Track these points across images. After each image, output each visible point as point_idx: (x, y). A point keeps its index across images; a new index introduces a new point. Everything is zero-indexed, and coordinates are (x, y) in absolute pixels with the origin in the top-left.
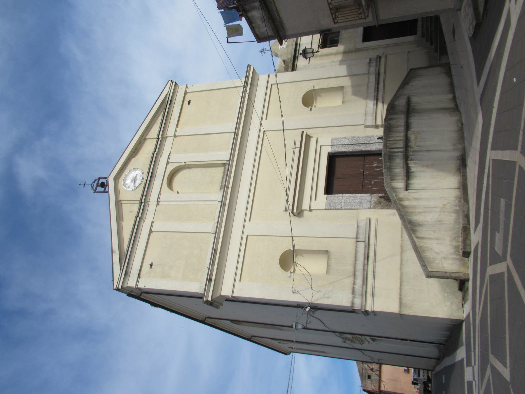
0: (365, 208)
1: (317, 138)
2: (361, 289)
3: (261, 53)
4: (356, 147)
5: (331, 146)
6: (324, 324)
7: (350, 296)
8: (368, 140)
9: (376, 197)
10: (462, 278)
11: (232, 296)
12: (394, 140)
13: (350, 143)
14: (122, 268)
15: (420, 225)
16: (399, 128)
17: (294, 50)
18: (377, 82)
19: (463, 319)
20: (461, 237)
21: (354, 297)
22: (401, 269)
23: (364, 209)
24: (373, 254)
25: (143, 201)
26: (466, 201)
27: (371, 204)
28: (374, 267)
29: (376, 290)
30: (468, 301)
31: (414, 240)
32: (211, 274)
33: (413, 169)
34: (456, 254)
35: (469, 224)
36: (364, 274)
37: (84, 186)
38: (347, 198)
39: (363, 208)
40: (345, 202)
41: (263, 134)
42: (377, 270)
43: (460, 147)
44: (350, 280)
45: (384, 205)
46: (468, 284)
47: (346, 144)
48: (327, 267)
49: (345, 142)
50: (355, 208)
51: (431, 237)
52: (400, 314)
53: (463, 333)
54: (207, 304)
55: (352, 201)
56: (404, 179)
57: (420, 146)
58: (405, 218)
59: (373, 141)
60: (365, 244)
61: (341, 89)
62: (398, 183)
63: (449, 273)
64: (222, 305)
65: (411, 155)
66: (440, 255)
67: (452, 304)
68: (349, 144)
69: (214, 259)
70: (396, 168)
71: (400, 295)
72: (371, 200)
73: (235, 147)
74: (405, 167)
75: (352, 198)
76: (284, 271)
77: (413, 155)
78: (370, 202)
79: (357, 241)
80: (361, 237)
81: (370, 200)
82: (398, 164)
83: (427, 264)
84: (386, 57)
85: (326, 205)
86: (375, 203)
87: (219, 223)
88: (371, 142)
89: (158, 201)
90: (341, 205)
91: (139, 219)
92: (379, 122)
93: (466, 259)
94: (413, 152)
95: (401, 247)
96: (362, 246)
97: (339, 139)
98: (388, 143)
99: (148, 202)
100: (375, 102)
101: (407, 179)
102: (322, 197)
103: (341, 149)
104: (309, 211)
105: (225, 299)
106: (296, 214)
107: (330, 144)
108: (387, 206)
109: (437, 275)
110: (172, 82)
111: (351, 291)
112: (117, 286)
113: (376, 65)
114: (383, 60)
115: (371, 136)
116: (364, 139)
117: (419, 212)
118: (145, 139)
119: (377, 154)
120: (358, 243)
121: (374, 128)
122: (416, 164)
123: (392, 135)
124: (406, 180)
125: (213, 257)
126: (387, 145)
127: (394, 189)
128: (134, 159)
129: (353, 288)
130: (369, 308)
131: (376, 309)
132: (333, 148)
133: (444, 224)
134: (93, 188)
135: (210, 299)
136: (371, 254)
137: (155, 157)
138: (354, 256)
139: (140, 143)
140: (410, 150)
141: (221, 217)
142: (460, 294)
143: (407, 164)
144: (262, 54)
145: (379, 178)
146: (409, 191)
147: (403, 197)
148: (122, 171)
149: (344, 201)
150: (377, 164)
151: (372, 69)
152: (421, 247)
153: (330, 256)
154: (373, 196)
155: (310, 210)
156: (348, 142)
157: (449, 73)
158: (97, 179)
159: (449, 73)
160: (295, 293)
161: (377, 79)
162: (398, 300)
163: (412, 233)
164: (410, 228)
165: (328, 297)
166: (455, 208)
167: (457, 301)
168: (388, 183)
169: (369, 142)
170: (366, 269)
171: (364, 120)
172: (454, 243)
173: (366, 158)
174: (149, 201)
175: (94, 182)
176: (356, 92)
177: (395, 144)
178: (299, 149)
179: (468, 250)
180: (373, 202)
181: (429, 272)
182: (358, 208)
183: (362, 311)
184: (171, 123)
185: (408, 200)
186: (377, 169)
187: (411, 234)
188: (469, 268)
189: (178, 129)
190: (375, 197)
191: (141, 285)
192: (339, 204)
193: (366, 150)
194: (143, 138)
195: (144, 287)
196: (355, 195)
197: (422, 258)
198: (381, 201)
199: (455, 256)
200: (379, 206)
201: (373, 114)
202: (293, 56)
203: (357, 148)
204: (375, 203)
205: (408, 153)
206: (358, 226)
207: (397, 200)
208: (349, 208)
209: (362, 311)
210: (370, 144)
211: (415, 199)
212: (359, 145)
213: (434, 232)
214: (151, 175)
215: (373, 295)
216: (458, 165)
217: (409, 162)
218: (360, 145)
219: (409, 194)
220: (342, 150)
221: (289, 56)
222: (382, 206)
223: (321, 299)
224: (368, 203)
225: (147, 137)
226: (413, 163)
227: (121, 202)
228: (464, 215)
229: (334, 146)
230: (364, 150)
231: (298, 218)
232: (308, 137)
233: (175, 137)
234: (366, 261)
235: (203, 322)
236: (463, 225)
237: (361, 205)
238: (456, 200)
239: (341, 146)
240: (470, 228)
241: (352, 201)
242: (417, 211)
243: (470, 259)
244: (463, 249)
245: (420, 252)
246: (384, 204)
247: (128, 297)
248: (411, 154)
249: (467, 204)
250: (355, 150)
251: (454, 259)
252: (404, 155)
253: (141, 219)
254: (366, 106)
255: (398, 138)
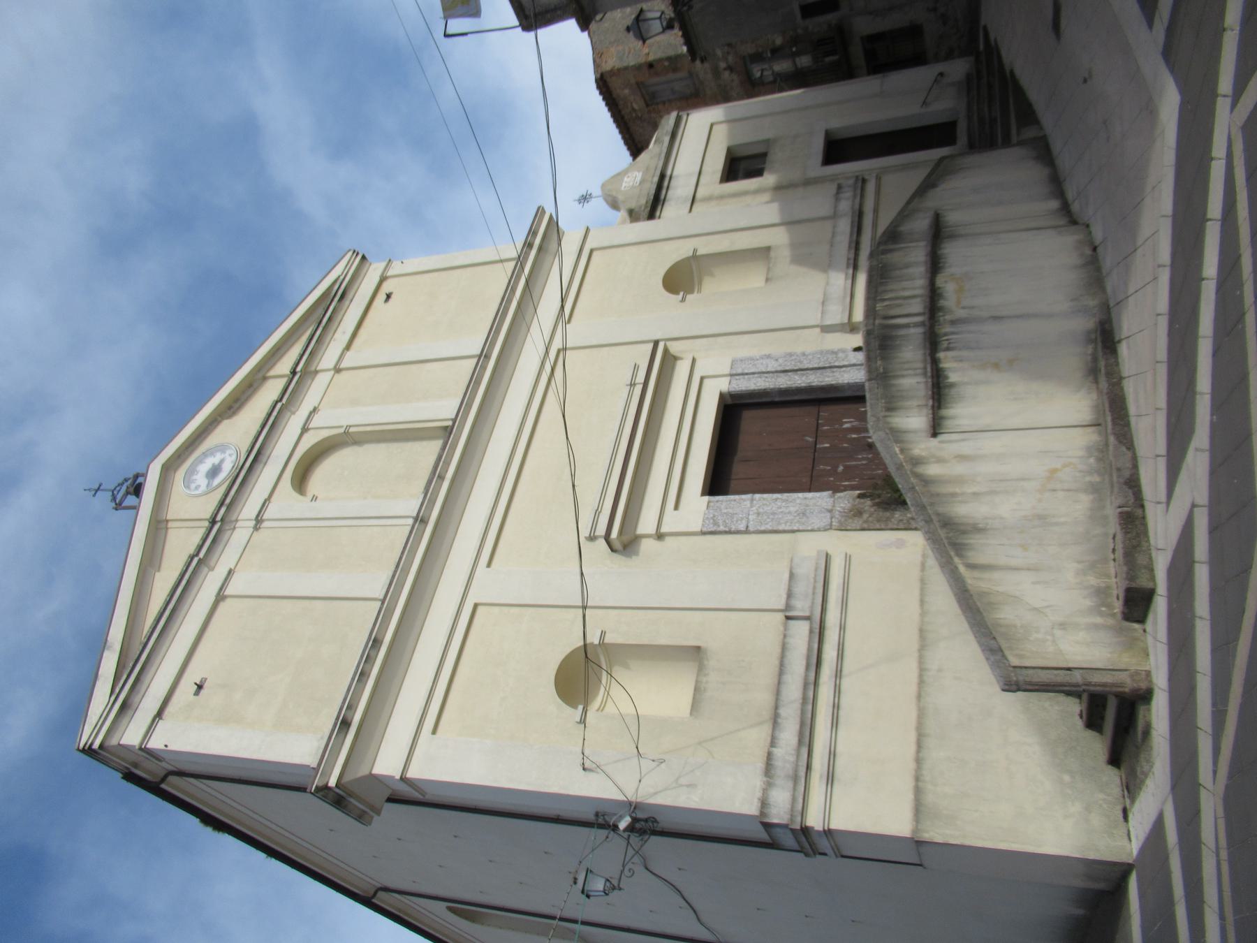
0: (816, 527)
1: (694, 360)
2: (792, 759)
3: (580, 203)
4: (797, 377)
5: (729, 378)
6: (695, 911)
7: (758, 782)
8: (829, 360)
9: (848, 500)
10: (1127, 690)
11: (401, 778)
12: (897, 298)
13: (779, 369)
14: (117, 690)
15: (977, 529)
16: (911, 270)
17: (654, 187)
18: (855, 229)
19: (1131, 862)
20: (1112, 562)
21: (769, 785)
22: (919, 697)
23: (812, 530)
24: (835, 654)
25: (219, 518)
26: (1125, 441)
27: (832, 518)
28: (837, 690)
29: (840, 762)
30: (1149, 782)
31: (960, 574)
32: (352, 707)
33: (953, 377)
34: (1101, 614)
35: (1142, 506)
36: (803, 712)
37: (95, 494)
38: (766, 504)
39: (810, 528)
40: (758, 514)
41: (555, 360)
42: (844, 701)
43: (1092, 303)
44: (764, 732)
45: (870, 519)
46: (1149, 710)
47: (768, 370)
48: (694, 695)
49: (767, 366)
50: (787, 528)
51: (1013, 562)
52: (916, 839)
53: (1129, 917)
54: (324, 799)
55: (780, 510)
56: (926, 405)
57: (972, 308)
58: (930, 512)
59: (843, 360)
60: (811, 623)
61: (764, 253)
62: (907, 417)
63: (1081, 671)
64: (378, 812)
65: (946, 334)
66: (1046, 616)
67: (1088, 809)
68: (777, 372)
69: (368, 666)
70: (903, 376)
71: (917, 779)
72: (834, 506)
73: (478, 383)
74: (929, 369)
75: (779, 504)
76: (564, 705)
77: (953, 333)
78: (830, 511)
79: (788, 618)
80: (801, 607)
81: (830, 508)
82: (908, 362)
83: (1004, 645)
84: (878, 179)
85: (704, 521)
86: (843, 514)
87: (400, 569)
88: (836, 364)
89: (259, 520)
90: (748, 522)
91: (198, 562)
92: (859, 315)
93: (1136, 626)
94: (953, 322)
95: (922, 632)
96: (801, 630)
97: (752, 359)
98: (879, 306)
99: (232, 522)
100: (851, 271)
101: (936, 404)
102: (696, 504)
103: (755, 384)
104: (655, 539)
105: (387, 794)
106: (617, 545)
107: (727, 371)
108: (878, 521)
109: (1040, 680)
110: (356, 253)
111: (760, 765)
112: (89, 738)
113: (855, 196)
114: (871, 187)
115: (839, 350)
116: (819, 358)
117: (975, 494)
118: (265, 379)
119: (851, 398)
120: (792, 622)
121: (846, 332)
122: (961, 361)
123: (890, 287)
124: (933, 407)
125: (368, 659)
126: (876, 311)
127: (897, 435)
128: (226, 423)
129: (770, 756)
130: (814, 820)
131: (839, 822)
132: (735, 382)
133: (1057, 524)
134: (114, 498)
135: (332, 782)
136: (830, 653)
137: (275, 413)
138: (777, 662)
139: (250, 386)
140: (945, 320)
141: (409, 551)
142: (1112, 777)
143: (935, 362)
144: (581, 204)
145: (860, 457)
146: (941, 438)
147: (923, 454)
148: (191, 448)
149: (756, 511)
150: (855, 424)
151: (845, 205)
152: (983, 594)
153: (706, 662)
154: (840, 497)
155: (660, 536)
156: (775, 366)
157: (1044, 153)
158: (131, 476)
159: (1044, 153)
160: (591, 770)
161: (856, 224)
162: (911, 796)
163: (952, 553)
164: (947, 538)
165: (688, 786)
166: (1088, 479)
167: (1104, 800)
168: (878, 419)
169: (832, 364)
170: (812, 696)
171: (820, 315)
172: (1092, 580)
173: (823, 408)
174: (237, 520)
175: (121, 485)
176: (803, 256)
177: (900, 306)
178: (641, 386)
179: (1143, 582)
180: (837, 513)
181: (1011, 669)
182: (795, 528)
183: (791, 829)
184: (334, 340)
185: (940, 460)
186: (854, 436)
187: (951, 557)
188: (1148, 655)
189: (349, 354)
190: (845, 500)
191: (155, 743)
192: (742, 519)
193: (823, 384)
194: (260, 375)
195: (162, 747)
196: (788, 496)
197: (987, 627)
198: (863, 508)
199: (1099, 620)
200: (858, 522)
201: (844, 297)
202: (652, 198)
203: (799, 381)
204: (843, 514)
205: (937, 327)
206: (792, 576)
207: (904, 464)
208: (770, 528)
209: (793, 827)
210: (835, 370)
211: (962, 458)
212: (805, 372)
213: (1024, 547)
214: (256, 457)
215: (830, 778)
216: (1089, 358)
217: (941, 355)
218: (808, 372)
219: (944, 445)
220: (758, 385)
221: (643, 201)
222: (866, 522)
223: (666, 789)
224: (822, 515)
225: (272, 373)
226: (953, 357)
227: (167, 524)
228: (1122, 480)
229: (737, 377)
230: (819, 384)
231: (623, 558)
232: (669, 361)
233: (337, 370)
234: (812, 675)
235: (366, 901)
236: (1120, 510)
237: (804, 519)
238: (1091, 456)
239: (756, 375)
240: (1144, 517)
241: (780, 510)
242: (970, 491)
243: (1149, 625)
244: (1127, 582)
245: (981, 610)
246: (870, 516)
247: (124, 782)
248: (948, 329)
249: (1128, 449)
250: (794, 386)
251: (1096, 627)
252: (925, 333)
253: (203, 565)
254: (827, 284)
255: (907, 293)
